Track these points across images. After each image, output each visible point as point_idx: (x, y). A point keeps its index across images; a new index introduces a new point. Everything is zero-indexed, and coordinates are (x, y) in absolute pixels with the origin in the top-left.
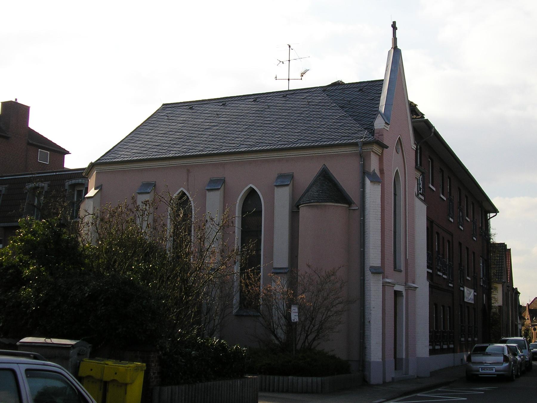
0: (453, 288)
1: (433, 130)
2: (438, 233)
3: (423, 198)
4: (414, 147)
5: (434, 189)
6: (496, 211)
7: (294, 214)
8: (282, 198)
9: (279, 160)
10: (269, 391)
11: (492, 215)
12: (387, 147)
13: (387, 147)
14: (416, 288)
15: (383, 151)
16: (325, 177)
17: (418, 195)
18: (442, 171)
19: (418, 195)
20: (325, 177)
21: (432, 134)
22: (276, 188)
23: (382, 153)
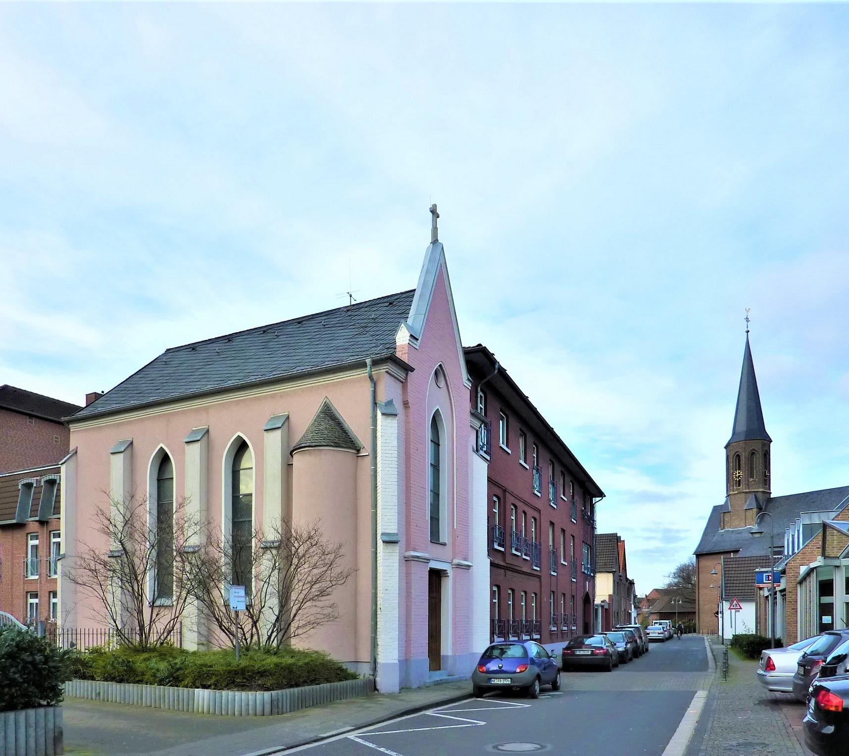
0: (540, 571)
1: (497, 366)
2: (525, 513)
3: (488, 458)
4: (469, 385)
5: (510, 452)
6: (601, 494)
7: (288, 467)
8: (274, 443)
9: (272, 396)
10: (695, 632)
11: (598, 499)
12: (412, 370)
13: (412, 370)
14: (469, 566)
15: (407, 375)
16: (328, 413)
17: (477, 450)
18: (563, 473)
19: (477, 450)
20: (328, 413)
21: (496, 371)
22: (265, 433)
23: (406, 379)
